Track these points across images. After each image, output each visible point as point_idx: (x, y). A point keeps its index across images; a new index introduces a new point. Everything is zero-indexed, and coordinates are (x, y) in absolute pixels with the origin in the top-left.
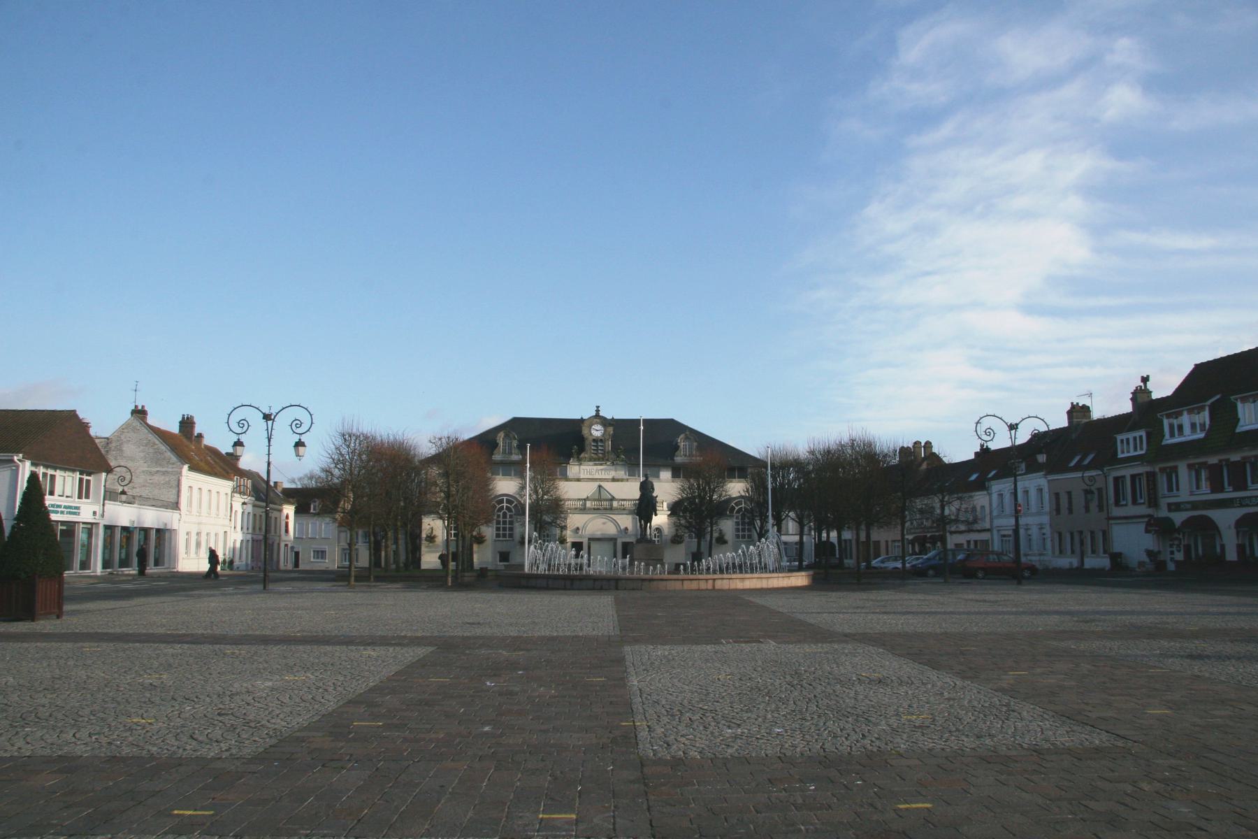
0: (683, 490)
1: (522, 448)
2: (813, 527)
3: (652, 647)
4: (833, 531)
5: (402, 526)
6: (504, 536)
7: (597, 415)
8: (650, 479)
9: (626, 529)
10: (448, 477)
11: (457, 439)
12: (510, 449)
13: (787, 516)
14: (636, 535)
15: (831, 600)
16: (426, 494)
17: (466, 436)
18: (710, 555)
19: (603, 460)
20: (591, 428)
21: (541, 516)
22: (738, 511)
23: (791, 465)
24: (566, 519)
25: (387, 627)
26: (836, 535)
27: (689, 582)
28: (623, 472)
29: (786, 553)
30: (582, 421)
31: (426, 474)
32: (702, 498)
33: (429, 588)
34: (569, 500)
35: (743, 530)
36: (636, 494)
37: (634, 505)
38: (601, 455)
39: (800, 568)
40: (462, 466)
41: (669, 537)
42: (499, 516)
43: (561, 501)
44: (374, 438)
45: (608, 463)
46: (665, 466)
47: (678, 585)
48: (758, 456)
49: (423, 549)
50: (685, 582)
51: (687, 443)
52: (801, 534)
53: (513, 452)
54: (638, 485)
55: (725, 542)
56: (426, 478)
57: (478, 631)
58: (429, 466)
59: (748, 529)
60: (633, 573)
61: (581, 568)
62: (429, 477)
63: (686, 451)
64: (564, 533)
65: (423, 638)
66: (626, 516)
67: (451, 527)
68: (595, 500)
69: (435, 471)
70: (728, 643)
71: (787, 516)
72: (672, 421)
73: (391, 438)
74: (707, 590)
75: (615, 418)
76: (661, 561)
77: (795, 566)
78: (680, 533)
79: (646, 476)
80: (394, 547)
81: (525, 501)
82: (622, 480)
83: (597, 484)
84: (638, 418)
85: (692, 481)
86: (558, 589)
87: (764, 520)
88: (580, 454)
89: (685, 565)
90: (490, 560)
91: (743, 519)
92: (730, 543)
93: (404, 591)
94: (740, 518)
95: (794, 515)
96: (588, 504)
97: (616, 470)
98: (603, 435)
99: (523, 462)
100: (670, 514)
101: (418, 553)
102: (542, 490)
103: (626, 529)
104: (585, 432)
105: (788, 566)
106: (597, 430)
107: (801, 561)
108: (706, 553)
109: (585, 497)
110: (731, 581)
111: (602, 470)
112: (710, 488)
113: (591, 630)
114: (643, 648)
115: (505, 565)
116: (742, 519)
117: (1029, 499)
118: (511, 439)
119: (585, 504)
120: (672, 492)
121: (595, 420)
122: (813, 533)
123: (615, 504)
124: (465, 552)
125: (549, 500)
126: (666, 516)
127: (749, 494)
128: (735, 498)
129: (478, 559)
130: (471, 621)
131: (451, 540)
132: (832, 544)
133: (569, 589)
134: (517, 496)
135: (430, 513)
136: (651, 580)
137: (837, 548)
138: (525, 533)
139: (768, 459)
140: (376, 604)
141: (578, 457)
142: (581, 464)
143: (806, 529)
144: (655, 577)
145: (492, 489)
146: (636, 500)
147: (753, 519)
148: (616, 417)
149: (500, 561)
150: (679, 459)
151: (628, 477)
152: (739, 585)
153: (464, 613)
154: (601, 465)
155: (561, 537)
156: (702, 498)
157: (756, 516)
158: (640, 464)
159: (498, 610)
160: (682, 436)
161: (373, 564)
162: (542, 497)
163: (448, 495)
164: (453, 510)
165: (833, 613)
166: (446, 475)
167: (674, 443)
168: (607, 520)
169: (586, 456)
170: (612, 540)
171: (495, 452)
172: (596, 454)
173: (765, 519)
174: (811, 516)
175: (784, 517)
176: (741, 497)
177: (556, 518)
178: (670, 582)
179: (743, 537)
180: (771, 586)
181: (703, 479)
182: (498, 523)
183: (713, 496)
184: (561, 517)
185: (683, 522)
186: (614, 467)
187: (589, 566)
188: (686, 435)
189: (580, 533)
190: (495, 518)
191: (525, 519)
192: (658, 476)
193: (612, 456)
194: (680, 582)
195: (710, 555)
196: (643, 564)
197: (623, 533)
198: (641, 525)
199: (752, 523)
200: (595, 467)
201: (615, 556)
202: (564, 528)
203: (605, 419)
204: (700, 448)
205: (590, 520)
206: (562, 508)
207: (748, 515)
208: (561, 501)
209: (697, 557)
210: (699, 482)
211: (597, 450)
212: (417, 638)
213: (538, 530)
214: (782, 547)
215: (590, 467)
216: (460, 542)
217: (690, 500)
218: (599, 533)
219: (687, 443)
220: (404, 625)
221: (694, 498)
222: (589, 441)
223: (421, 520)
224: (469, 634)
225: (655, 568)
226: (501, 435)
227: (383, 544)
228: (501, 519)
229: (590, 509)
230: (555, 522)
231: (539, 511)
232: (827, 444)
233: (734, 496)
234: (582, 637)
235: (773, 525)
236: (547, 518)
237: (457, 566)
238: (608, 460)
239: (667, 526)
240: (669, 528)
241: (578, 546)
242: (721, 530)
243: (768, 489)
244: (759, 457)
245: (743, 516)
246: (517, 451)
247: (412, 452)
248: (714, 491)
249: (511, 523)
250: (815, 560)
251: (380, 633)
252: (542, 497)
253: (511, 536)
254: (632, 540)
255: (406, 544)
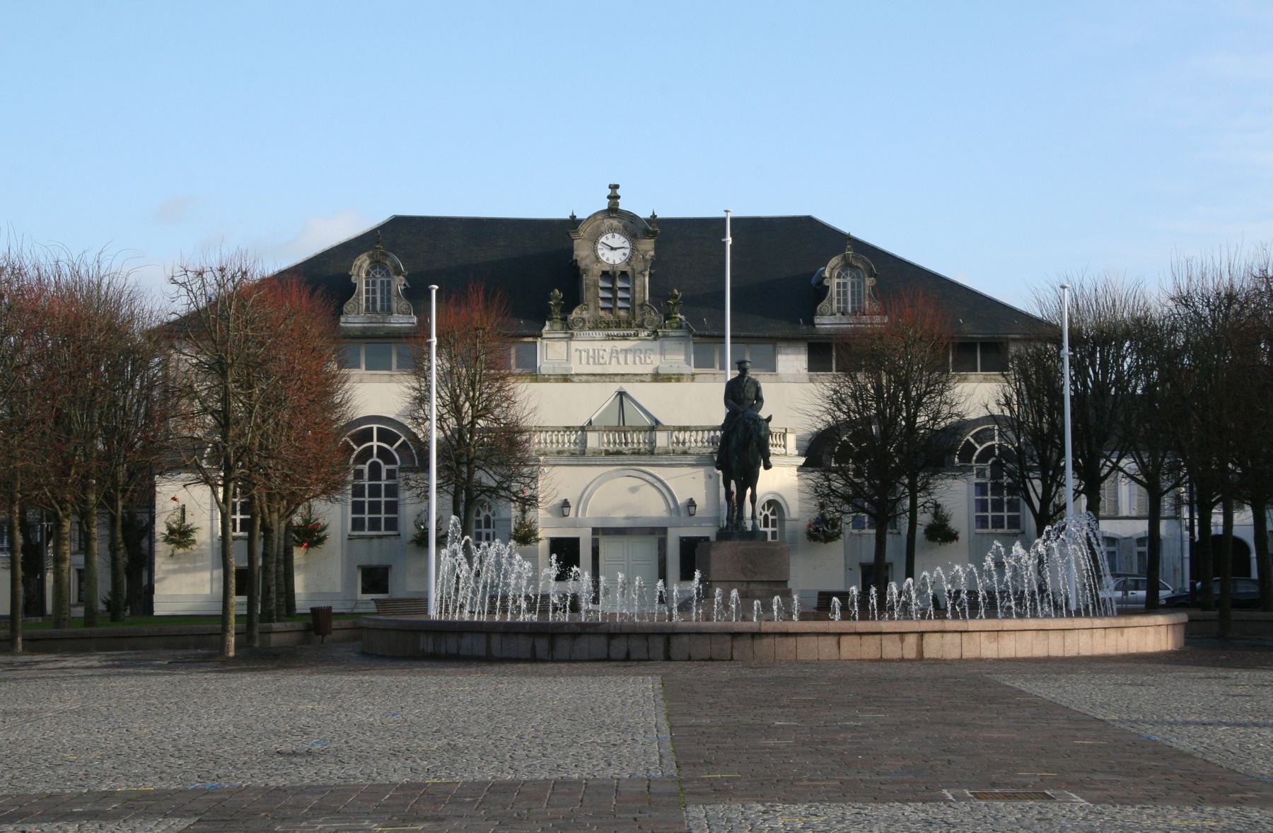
0: (838, 401)
1: (416, 296)
2: (1185, 496)
3: (761, 808)
4: (1241, 508)
5: (100, 505)
6: (375, 524)
7: (613, 210)
8: (752, 373)
9: (691, 503)
10: (223, 374)
11: (245, 273)
12: (387, 298)
13: (1116, 467)
14: (718, 519)
15: (1239, 690)
16: (164, 418)
17: (270, 266)
18: (910, 573)
19: (629, 326)
20: (595, 242)
21: (471, 474)
22: (984, 457)
23: (1127, 334)
24: (534, 479)
25: (61, 771)
26: (1251, 520)
27: (856, 639)
28: (682, 357)
29: (1112, 567)
30: (573, 223)
31: (165, 365)
32: (888, 424)
33: (174, 665)
34: (541, 429)
35: (997, 506)
36: (718, 415)
37: (712, 441)
38: (622, 313)
39: (1152, 606)
40: (262, 344)
41: (802, 526)
42: (359, 474)
43: (521, 432)
44: (18, 272)
45: (643, 334)
46: (791, 340)
47: (826, 648)
48: (1035, 312)
49: (161, 564)
50: (844, 640)
51: (849, 280)
52: (1154, 517)
53: (394, 305)
54: (720, 389)
55: (951, 536)
56: (166, 376)
57: (307, 774)
58: (172, 347)
59: (1009, 502)
60: (708, 618)
61: (575, 607)
62: (172, 373)
63: (845, 301)
64: (530, 515)
65: (159, 795)
66: (690, 470)
67: (234, 505)
68: (609, 429)
69: (185, 360)
70: (958, 798)
71: (1116, 467)
72: (809, 221)
73: (66, 271)
74: (902, 660)
75: (660, 215)
76: (780, 586)
77: (1136, 601)
78: (831, 512)
79: (741, 365)
80: (80, 559)
81: (428, 434)
82: (679, 378)
83: (614, 387)
84: (721, 214)
85: (861, 377)
86: (517, 660)
87: (1052, 478)
88: (570, 312)
89: (844, 596)
90: (339, 589)
91: (996, 475)
92: (963, 535)
93: (108, 675)
94: (988, 473)
95: (1134, 466)
96: (593, 440)
97: (663, 352)
98: (629, 262)
99: (424, 327)
100: (805, 465)
101: (145, 574)
102: (472, 406)
103: (691, 503)
104: (581, 252)
105: (1119, 601)
106: (612, 249)
107: (1153, 588)
108: (900, 566)
109: (582, 422)
110: (965, 635)
111: (626, 351)
112: (907, 396)
113: (603, 765)
114: (735, 810)
115: (376, 601)
116: (992, 478)
117: (694, 631)
118: (388, 275)
119: (584, 442)
120: (810, 408)
121: (608, 222)
122: (1186, 513)
123: (662, 439)
124: (273, 568)
125: (489, 430)
126: (794, 471)
127: (1012, 411)
128: (977, 422)
129: (306, 587)
130: (287, 747)
131: (235, 539)
132: (1240, 544)
133: (543, 661)
134: (408, 422)
135: (176, 467)
136: (756, 635)
137: (1254, 555)
138: (428, 519)
139: (1061, 317)
140: (30, 713)
141: (564, 319)
142: (571, 338)
143: (1167, 502)
144: (767, 627)
145: (340, 405)
146: (715, 429)
147: (1024, 477)
148: (662, 214)
149: (364, 591)
150: (826, 322)
151: (694, 370)
152: (987, 648)
153: (271, 726)
154: (625, 338)
155: (522, 525)
156: (888, 424)
157: (1031, 469)
158: (724, 337)
159: (359, 717)
160: (835, 261)
161: (21, 601)
162: (473, 423)
163: (224, 421)
164: (237, 461)
165: (1245, 725)
166: (219, 368)
167: (814, 281)
168: (639, 482)
169: (585, 315)
170: (657, 532)
171: (347, 307)
172: (610, 310)
173: (1053, 478)
174: (1180, 468)
175: (1105, 470)
176: (993, 418)
177: (510, 478)
178: (806, 638)
179: (998, 523)
180: (1071, 652)
181: (889, 373)
182: (358, 491)
183: (915, 416)
184: (521, 475)
185: (838, 484)
186: (656, 344)
187: (596, 600)
188: (845, 258)
189: (572, 514)
190: (350, 478)
191: (428, 479)
192: (772, 368)
193: (654, 316)
194: (832, 641)
195: (910, 573)
196: (734, 593)
197: (683, 514)
198: (729, 494)
199: (1019, 488)
200: (609, 345)
201: (663, 575)
202: (529, 502)
203: (632, 218)
204: (880, 293)
205: (600, 481)
206: (526, 451)
207: (1010, 466)
208: (521, 432)
209: (875, 574)
210: (879, 379)
211: (613, 300)
212: (145, 795)
213: (462, 508)
214: (1101, 550)
215: (597, 345)
216: (259, 547)
217: (858, 428)
218: (621, 514)
219: (849, 280)
220: (108, 764)
221: (869, 421)
222: (591, 278)
223: (153, 486)
224: (282, 782)
225: (767, 607)
226: (362, 263)
227: (50, 553)
228: (366, 483)
229: (596, 453)
230: (508, 489)
231: (465, 459)
232: (1226, 277)
233: (973, 416)
234: (578, 782)
235: (1077, 493)
236: (485, 478)
237: (251, 605)
238: (641, 326)
239: (796, 495)
240: (801, 500)
241: (565, 551)
242: (937, 506)
243: (1062, 397)
244: (1039, 315)
245: (997, 469)
246: (404, 304)
247: (124, 310)
248: (919, 404)
249: (392, 491)
250: (1193, 586)
251: (40, 787)
252: (473, 423)
253: (392, 524)
254: (708, 531)
255: (113, 548)
